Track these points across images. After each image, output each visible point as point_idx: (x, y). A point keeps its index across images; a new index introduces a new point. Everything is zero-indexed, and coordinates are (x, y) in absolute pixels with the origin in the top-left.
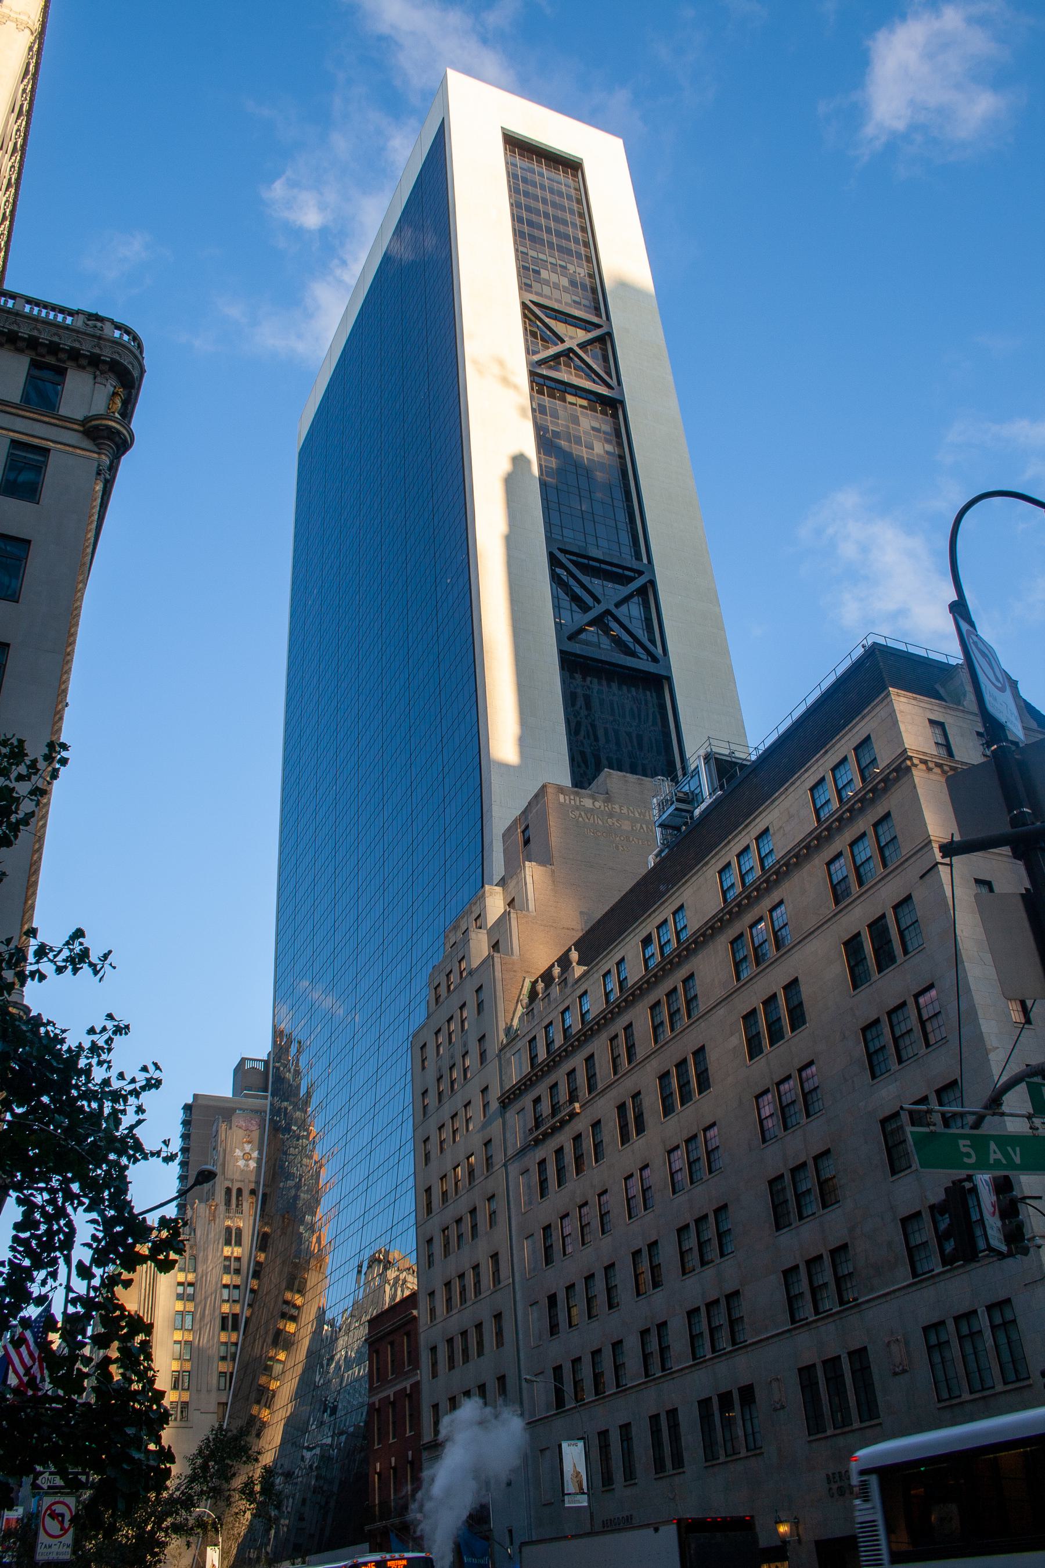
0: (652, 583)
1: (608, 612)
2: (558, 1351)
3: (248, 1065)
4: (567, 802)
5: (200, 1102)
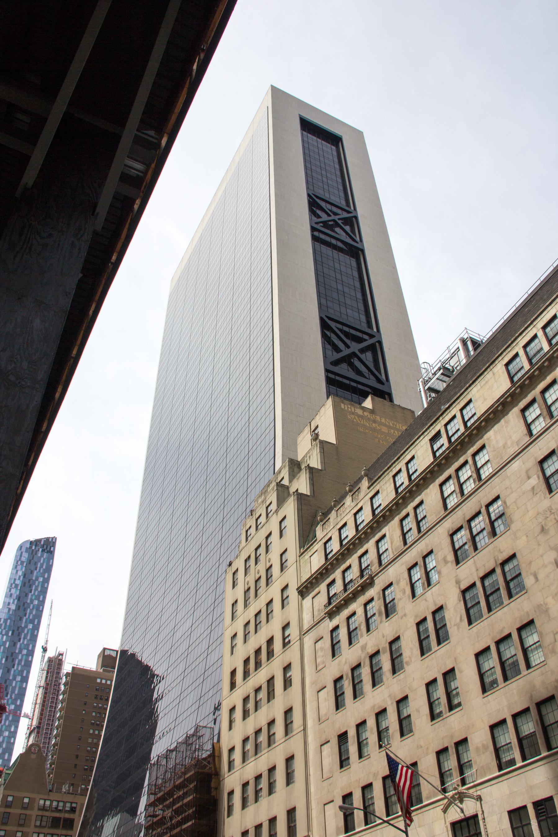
0: (380, 343)
1: (354, 354)
3: (107, 653)
4: (346, 408)
5: (75, 672)
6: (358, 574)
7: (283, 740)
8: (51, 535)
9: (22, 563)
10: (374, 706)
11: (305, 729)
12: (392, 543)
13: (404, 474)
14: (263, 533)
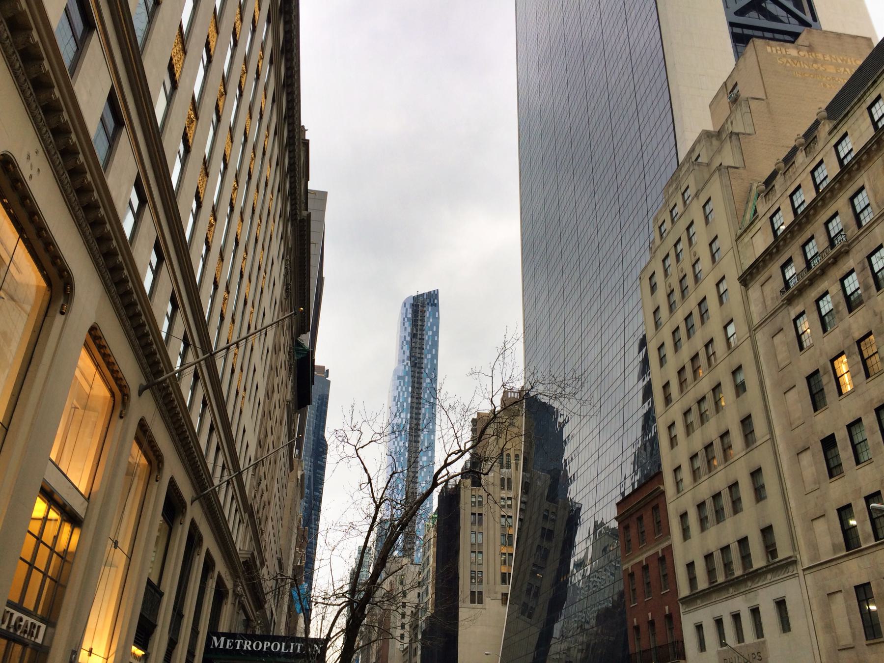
2: (838, 492)
4: (774, 51)
6: (827, 244)
7: (744, 453)
8: (431, 289)
9: (408, 319)
10: (872, 400)
11: (772, 438)
12: (875, 196)
13: (809, 185)
14: (682, 224)
